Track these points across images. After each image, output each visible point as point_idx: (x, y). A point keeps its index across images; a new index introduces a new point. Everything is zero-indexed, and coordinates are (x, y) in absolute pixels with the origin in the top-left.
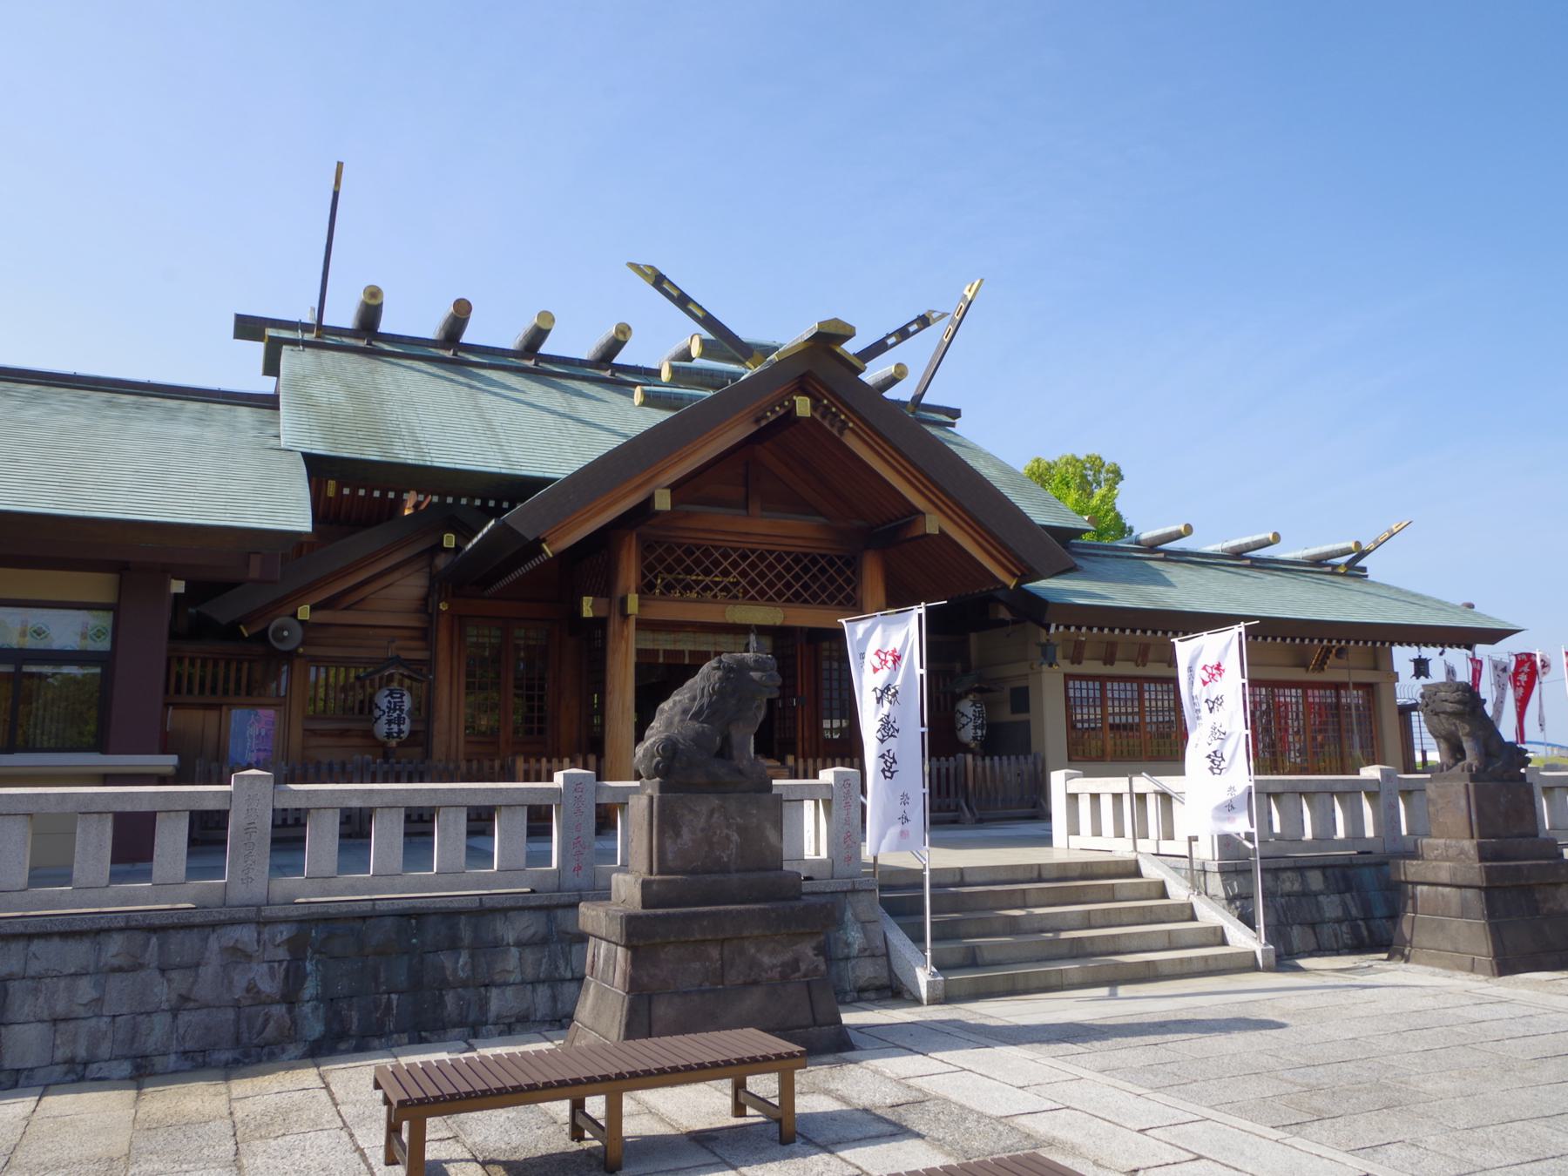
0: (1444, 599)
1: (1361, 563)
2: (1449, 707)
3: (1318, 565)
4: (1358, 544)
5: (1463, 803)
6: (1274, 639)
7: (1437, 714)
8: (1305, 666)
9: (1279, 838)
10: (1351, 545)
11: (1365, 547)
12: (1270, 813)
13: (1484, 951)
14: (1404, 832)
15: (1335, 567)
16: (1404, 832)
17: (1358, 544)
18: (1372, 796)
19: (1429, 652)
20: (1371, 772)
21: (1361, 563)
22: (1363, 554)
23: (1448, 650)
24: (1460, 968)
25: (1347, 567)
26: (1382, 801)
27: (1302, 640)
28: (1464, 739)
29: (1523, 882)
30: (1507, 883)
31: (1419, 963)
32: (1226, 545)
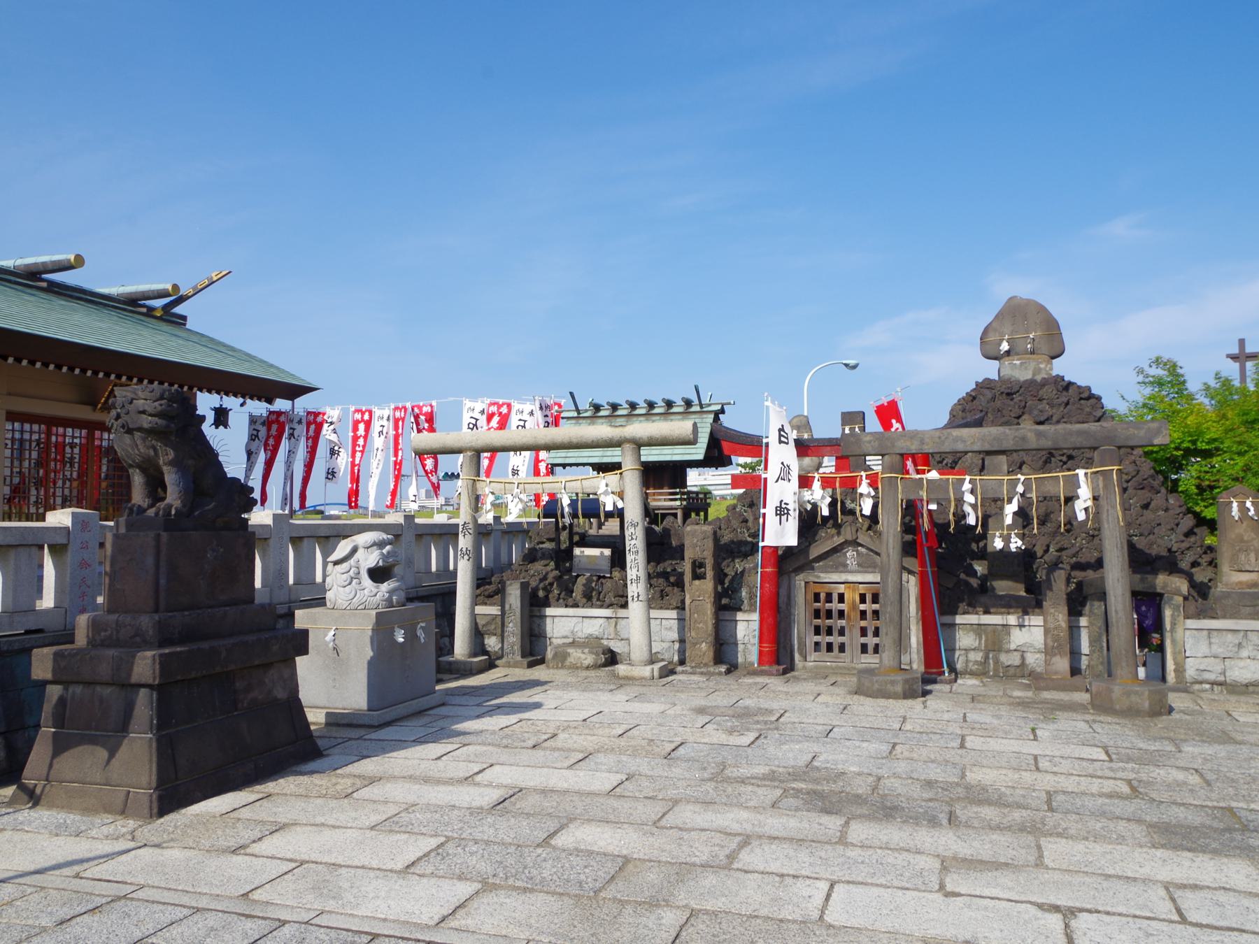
0: (253, 354)
1: (178, 310)
2: (146, 422)
3: (132, 305)
4: (176, 287)
5: (150, 560)
6: (59, 367)
7: (130, 431)
8: (94, 404)
9: (485, 570)
10: (169, 287)
11: (184, 291)
12: (41, 566)
13: (144, 780)
14: (291, 581)
15: (151, 309)
16: (291, 581)
17: (176, 287)
18: (57, 550)
19: (231, 402)
20: (60, 518)
21: (178, 310)
22: (181, 300)
23: (248, 401)
24: (107, 809)
25: (166, 311)
26: (69, 557)
27: (96, 373)
28: (165, 469)
29: (218, 669)
30: (193, 675)
31: (51, 806)
32: (19, 262)
